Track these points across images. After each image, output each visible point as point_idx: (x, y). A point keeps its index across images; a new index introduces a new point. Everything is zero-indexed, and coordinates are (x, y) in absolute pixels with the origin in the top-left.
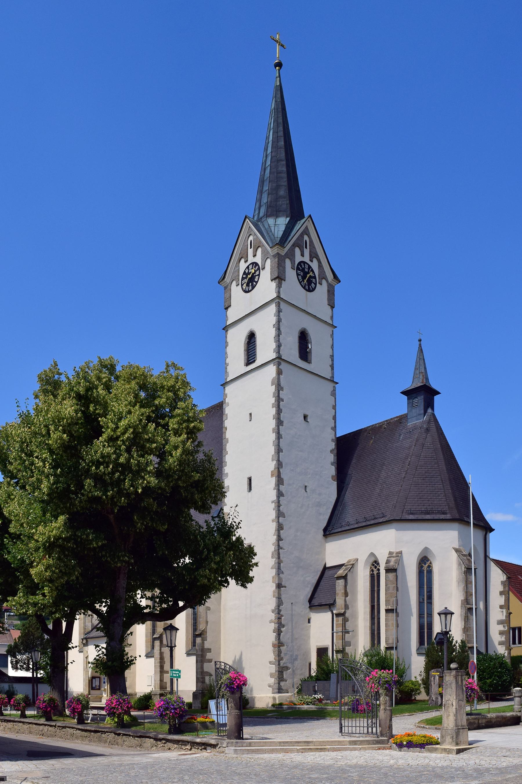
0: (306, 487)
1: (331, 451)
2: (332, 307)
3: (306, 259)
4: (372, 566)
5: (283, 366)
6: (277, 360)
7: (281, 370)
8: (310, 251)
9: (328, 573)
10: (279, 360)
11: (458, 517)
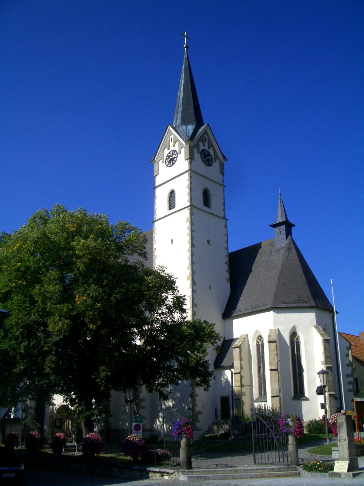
1: (226, 263)
3: (206, 148)
8: (208, 143)
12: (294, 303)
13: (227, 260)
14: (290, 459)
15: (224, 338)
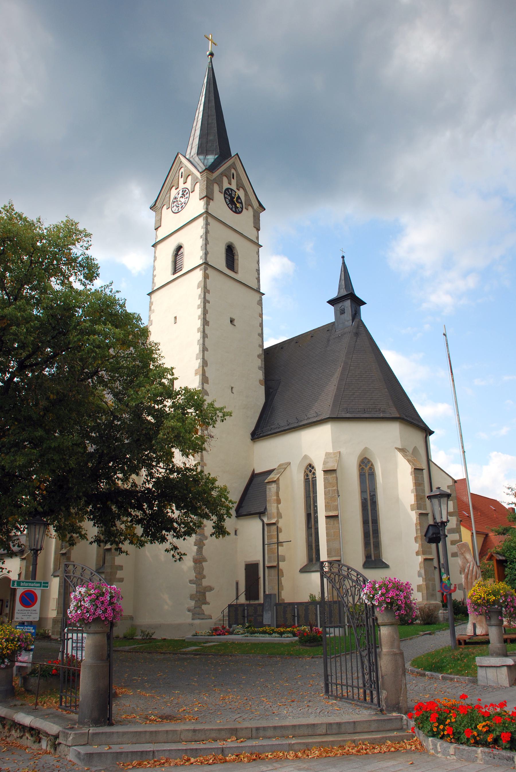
0: (232, 388)
1: (259, 356)
2: (258, 229)
3: (234, 187)
4: (306, 471)
5: (210, 271)
6: (203, 266)
7: (208, 274)
8: (237, 182)
9: (256, 481)
10: (206, 265)
11: (398, 416)
12: (364, 411)
13: (261, 353)
14: (384, 694)
15: (254, 470)
